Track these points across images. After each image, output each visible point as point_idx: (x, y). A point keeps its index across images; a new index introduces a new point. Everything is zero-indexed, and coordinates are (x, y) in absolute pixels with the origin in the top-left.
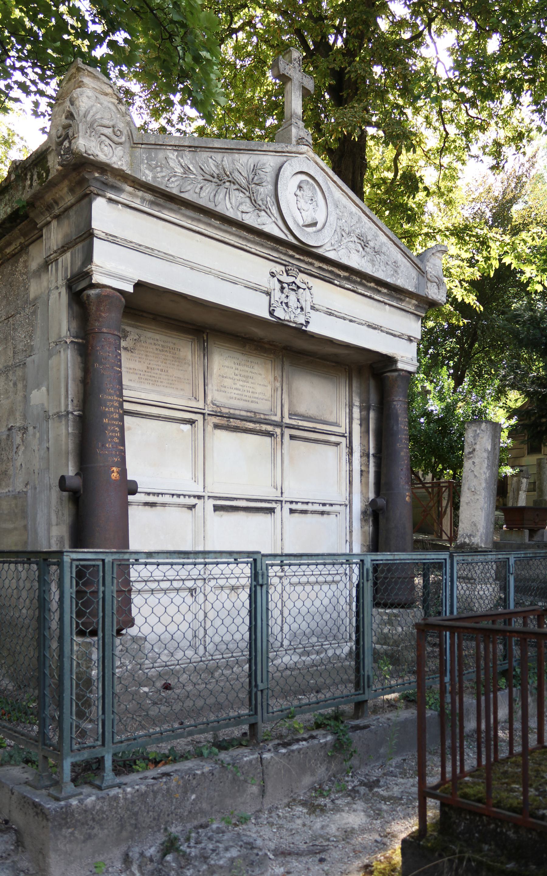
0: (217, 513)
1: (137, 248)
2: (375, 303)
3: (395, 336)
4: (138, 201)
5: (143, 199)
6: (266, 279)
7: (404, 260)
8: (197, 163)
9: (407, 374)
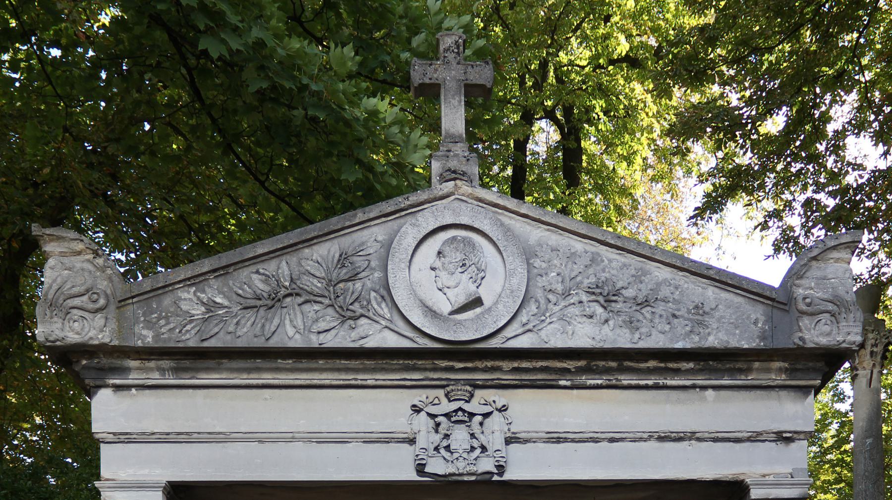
1: (165, 438)
3: (737, 440)
4: (157, 375)
5: (162, 370)
6: (403, 420)
7: (724, 295)
8: (231, 289)
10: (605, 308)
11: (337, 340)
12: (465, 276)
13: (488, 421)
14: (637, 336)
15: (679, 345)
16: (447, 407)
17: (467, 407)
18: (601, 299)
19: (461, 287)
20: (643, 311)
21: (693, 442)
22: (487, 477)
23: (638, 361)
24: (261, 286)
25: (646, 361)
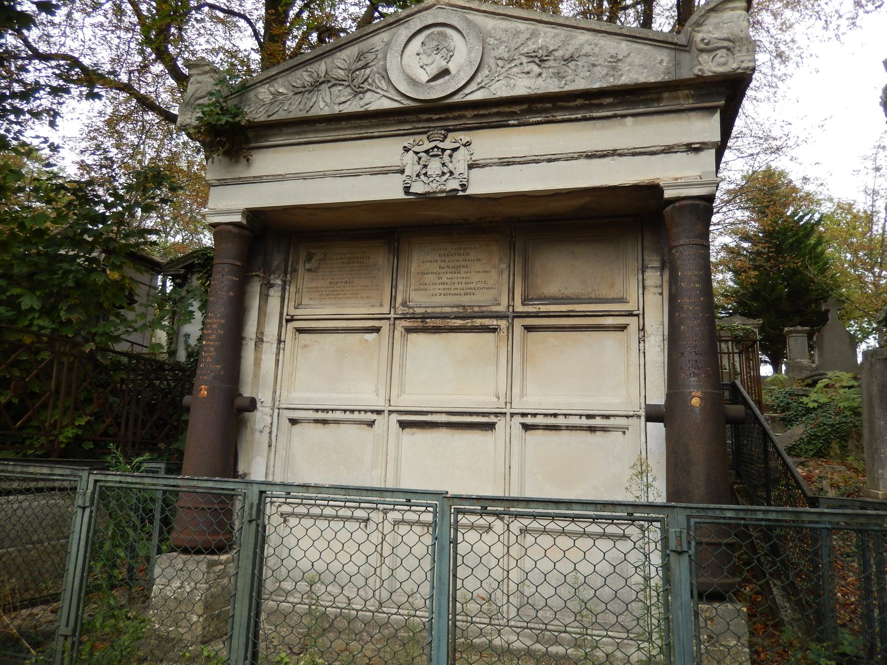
0: (407, 430)
2: (599, 123)
6: (398, 157)
9: (702, 203)
10: (539, 66)
11: (351, 107)
12: (438, 56)
13: (455, 154)
14: (563, 82)
15: (597, 86)
16: (428, 145)
17: (441, 145)
18: (537, 60)
19: (435, 63)
20: (569, 64)
21: (616, 157)
22: (454, 193)
23: (567, 102)
24: (308, 79)
25: (575, 101)
